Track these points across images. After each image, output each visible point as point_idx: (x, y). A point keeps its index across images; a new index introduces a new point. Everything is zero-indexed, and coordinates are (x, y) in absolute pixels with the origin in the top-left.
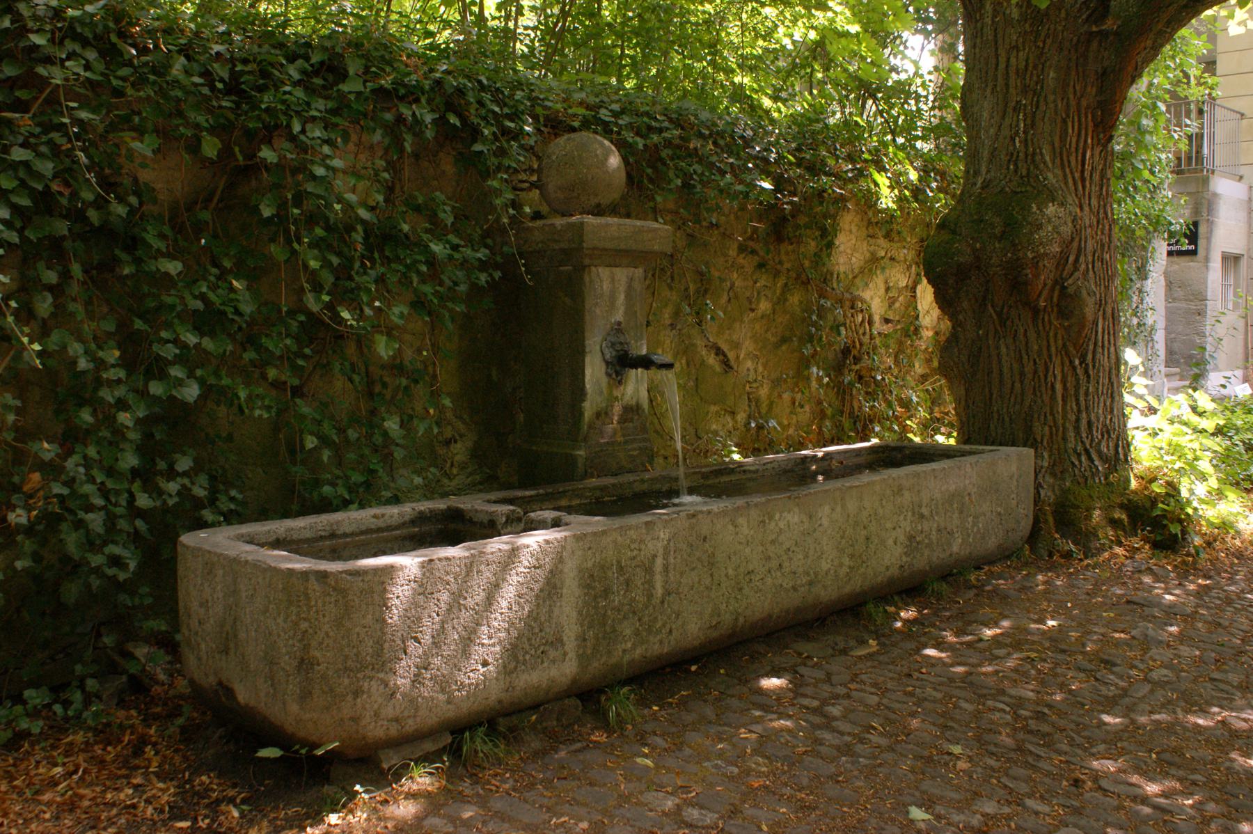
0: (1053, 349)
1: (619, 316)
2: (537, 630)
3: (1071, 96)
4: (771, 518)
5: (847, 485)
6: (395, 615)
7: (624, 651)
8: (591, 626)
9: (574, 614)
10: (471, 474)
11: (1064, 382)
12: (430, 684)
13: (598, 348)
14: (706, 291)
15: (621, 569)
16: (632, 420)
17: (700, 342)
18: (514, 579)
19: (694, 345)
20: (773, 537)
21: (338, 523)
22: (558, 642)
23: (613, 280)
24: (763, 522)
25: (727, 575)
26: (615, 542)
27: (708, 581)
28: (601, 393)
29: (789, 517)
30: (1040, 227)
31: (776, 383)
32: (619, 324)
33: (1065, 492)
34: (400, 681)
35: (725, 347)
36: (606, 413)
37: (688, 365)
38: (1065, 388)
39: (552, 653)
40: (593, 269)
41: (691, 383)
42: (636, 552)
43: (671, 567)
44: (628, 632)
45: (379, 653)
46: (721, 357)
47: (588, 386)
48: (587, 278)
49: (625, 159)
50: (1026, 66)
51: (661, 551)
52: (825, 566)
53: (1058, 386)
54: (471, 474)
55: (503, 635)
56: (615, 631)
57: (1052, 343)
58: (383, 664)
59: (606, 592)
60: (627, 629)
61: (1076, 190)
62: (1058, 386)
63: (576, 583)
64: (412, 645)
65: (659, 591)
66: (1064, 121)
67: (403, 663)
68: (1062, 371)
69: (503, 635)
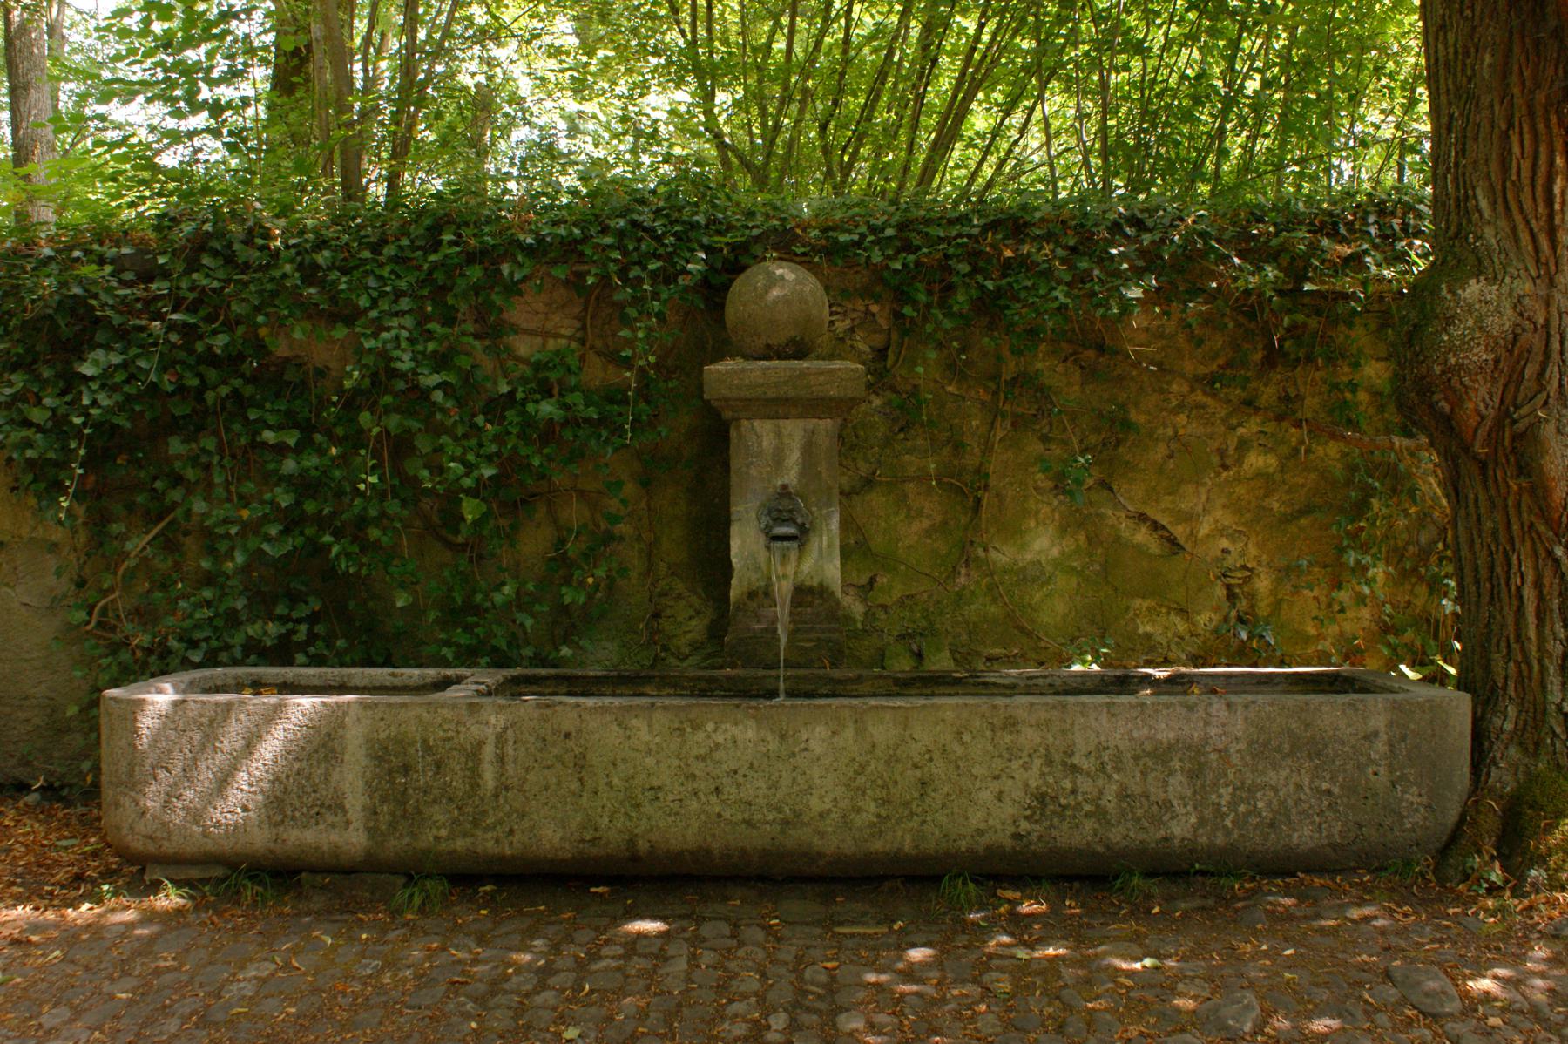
0: (1515, 528)
1: (791, 476)
2: (309, 790)
3: (1516, 91)
6: (144, 742)
7: (437, 838)
8: (384, 800)
9: (360, 784)
10: (709, 656)
11: (1538, 584)
12: (182, 814)
15: (428, 749)
16: (811, 605)
18: (279, 733)
20: (702, 751)
21: (349, 676)
22: (339, 807)
23: (778, 434)
24: (681, 730)
25: (609, 784)
26: (419, 718)
27: (575, 786)
30: (1449, 321)
31: (1286, 572)
32: (784, 487)
33: (1532, 778)
34: (150, 804)
38: (1541, 598)
39: (330, 818)
40: (745, 422)
42: (450, 734)
43: (509, 760)
45: (131, 774)
47: (734, 561)
48: (733, 434)
50: (1456, 53)
51: (491, 739)
52: (816, 804)
53: (1529, 593)
54: (709, 656)
55: (266, 786)
56: (420, 812)
57: (1514, 520)
58: (134, 785)
59: (406, 769)
60: (439, 814)
61: (1537, 250)
62: (1529, 593)
63: (363, 751)
64: (162, 774)
66: (1505, 136)
67: (153, 788)
68: (1536, 568)
69: (266, 786)
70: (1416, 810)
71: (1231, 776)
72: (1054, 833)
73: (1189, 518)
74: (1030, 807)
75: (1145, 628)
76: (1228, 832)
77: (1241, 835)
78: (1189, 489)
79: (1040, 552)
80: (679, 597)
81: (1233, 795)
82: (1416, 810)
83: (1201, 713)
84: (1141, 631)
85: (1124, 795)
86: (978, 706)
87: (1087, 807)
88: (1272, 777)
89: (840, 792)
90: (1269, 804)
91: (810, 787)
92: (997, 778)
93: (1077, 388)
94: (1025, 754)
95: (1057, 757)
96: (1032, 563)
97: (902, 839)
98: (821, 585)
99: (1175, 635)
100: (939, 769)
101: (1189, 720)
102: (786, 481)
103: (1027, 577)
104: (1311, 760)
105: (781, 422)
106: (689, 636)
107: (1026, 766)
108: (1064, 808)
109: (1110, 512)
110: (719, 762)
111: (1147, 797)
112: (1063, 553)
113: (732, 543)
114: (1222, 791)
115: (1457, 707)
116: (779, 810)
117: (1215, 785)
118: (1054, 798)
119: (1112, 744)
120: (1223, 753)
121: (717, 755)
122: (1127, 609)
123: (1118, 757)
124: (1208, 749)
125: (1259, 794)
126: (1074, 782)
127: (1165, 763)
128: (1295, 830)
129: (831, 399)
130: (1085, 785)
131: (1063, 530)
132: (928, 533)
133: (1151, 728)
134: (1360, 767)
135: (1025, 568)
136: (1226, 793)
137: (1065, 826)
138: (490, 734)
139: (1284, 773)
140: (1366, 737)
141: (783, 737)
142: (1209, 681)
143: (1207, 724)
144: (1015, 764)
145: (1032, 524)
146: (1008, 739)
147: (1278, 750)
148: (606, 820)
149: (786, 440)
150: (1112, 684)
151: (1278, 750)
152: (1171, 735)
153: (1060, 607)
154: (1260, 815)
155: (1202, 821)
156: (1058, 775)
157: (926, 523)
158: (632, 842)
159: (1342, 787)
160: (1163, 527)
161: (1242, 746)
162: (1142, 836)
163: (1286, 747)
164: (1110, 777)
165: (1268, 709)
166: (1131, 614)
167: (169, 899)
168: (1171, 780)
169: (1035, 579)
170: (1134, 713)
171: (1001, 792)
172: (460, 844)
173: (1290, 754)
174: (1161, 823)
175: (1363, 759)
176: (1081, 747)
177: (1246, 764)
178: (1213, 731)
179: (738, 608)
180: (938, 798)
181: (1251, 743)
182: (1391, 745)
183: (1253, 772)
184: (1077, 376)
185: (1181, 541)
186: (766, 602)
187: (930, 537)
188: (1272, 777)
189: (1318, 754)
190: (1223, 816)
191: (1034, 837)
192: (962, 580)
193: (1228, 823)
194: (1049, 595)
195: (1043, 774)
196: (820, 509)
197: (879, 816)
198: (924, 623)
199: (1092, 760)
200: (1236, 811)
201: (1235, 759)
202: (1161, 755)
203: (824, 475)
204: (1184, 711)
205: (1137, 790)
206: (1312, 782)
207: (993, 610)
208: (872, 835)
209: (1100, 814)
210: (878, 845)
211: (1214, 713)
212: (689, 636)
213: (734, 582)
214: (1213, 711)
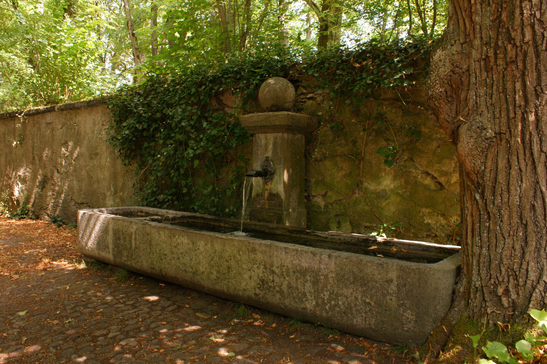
1: (269, 154)
4: (174, 236)
5: (217, 235)
16: (274, 200)
20: (175, 245)
22: (108, 247)
23: (266, 139)
28: (260, 186)
29: (183, 239)
32: (266, 157)
36: (262, 195)
40: (257, 135)
44: (125, 254)
65: (134, 246)
70: (410, 322)
71: (329, 288)
72: (267, 296)
73: (445, 174)
74: (259, 284)
75: (427, 221)
76: (327, 312)
77: (333, 314)
78: (447, 161)
81: (329, 296)
82: (410, 322)
83: (318, 257)
84: (425, 222)
85: (290, 287)
86: (244, 241)
87: (277, 289)
88: (345, 291)
89: (207, 266)
90: (344, 303)
91: (200, 263)
92: (250, 270)
93: (400, 118)
94: (258, 263)
95: (268, 266)
96: (383, 190)
97: (222, 287)
98: (277, 193)
99: (441, 225)
100: (233, 263)
101: (313, 260)
102: (268, 155)
103: (382, 195)
104: (362, 287)
105: (267, 134)
107: (258, 268)
108: (270, 287)
109: (414, 171)
110: (179, 249)
111: (298, 289)
112: (395, 187)
114: (325, 293)
115: (433, 274)
116: (192, 268)
117: (322, 290)
118: (267, 283)
119: (286, 264)
120: (326, 277)
121: (179, 247)
122: (420, 212)
123: (288, 270)
124: (320, 274)
125: (340, 298)
126: (273, 277)
127: (304, 276)
128: (355, 318)
130: (277, 280)
131: (395, 178)
132: (345, 176)
133: (300, 260)
134: (384, 295)
135: (379, 192)
136: (327, 294)
137: (270, 294)
138: (133, 230)
139: (351, 291)
140: (387, 281)
141: (193, 243)
142: (401, 246)
143: (320, 263)
144: (255, 266)
145: (383, 174)
146: (253, 256)
147: (348, 279)
148: (155, 263)
150: (362, 242)
151: (348, 279)
152: (307, 265)
153: (393, 209)
154: (340, 307)
155: (317, 304)
156: (268, 273)
157: (344, 173)
158: (161, 270)
159: (375, 302)
160: (436, 178)
161: (333, 275)
162: (296, 305)
163: (352, 279)
164: (285, 278)
165: (345, 260)
166: (421, 214)
167: (83, 266)
168: (306, 284)
169: (383, 197)
170: (294, 253)
171: (251, 276)
172: (129, 263)
173: (353, 283)
174: (302, 301)
175: (385, 292)
176: (276, 264)
177: (335, 284)
178: (322, 266)
180: (233, 273)
181: (337, 274)
182: (398, 286)
183: (337, 287)
184: (401, 114)
185: (444, 184)
186: (262, 198)
187: (345, 178)
188: (345, 291)
189: (365, 285)
190: (326, 304)
191: (261, 296)
192: (357, 195)
193: (327, 307)
194: (388, 204)
195: (263, 272)
197: (217, 277)
198: (344, 211)
199: (279, 270)
200: (330, 303)
201: (331, 280)
202: (303, 272)
203: (279, 154)
204: (312, 255)
205: (294, 285)
206: (362, 297)
207: (366, 208)
208: (215, 283)
209: (281, 292)
210: (217, 287)
211: (323, 258)
214: (323, 257)
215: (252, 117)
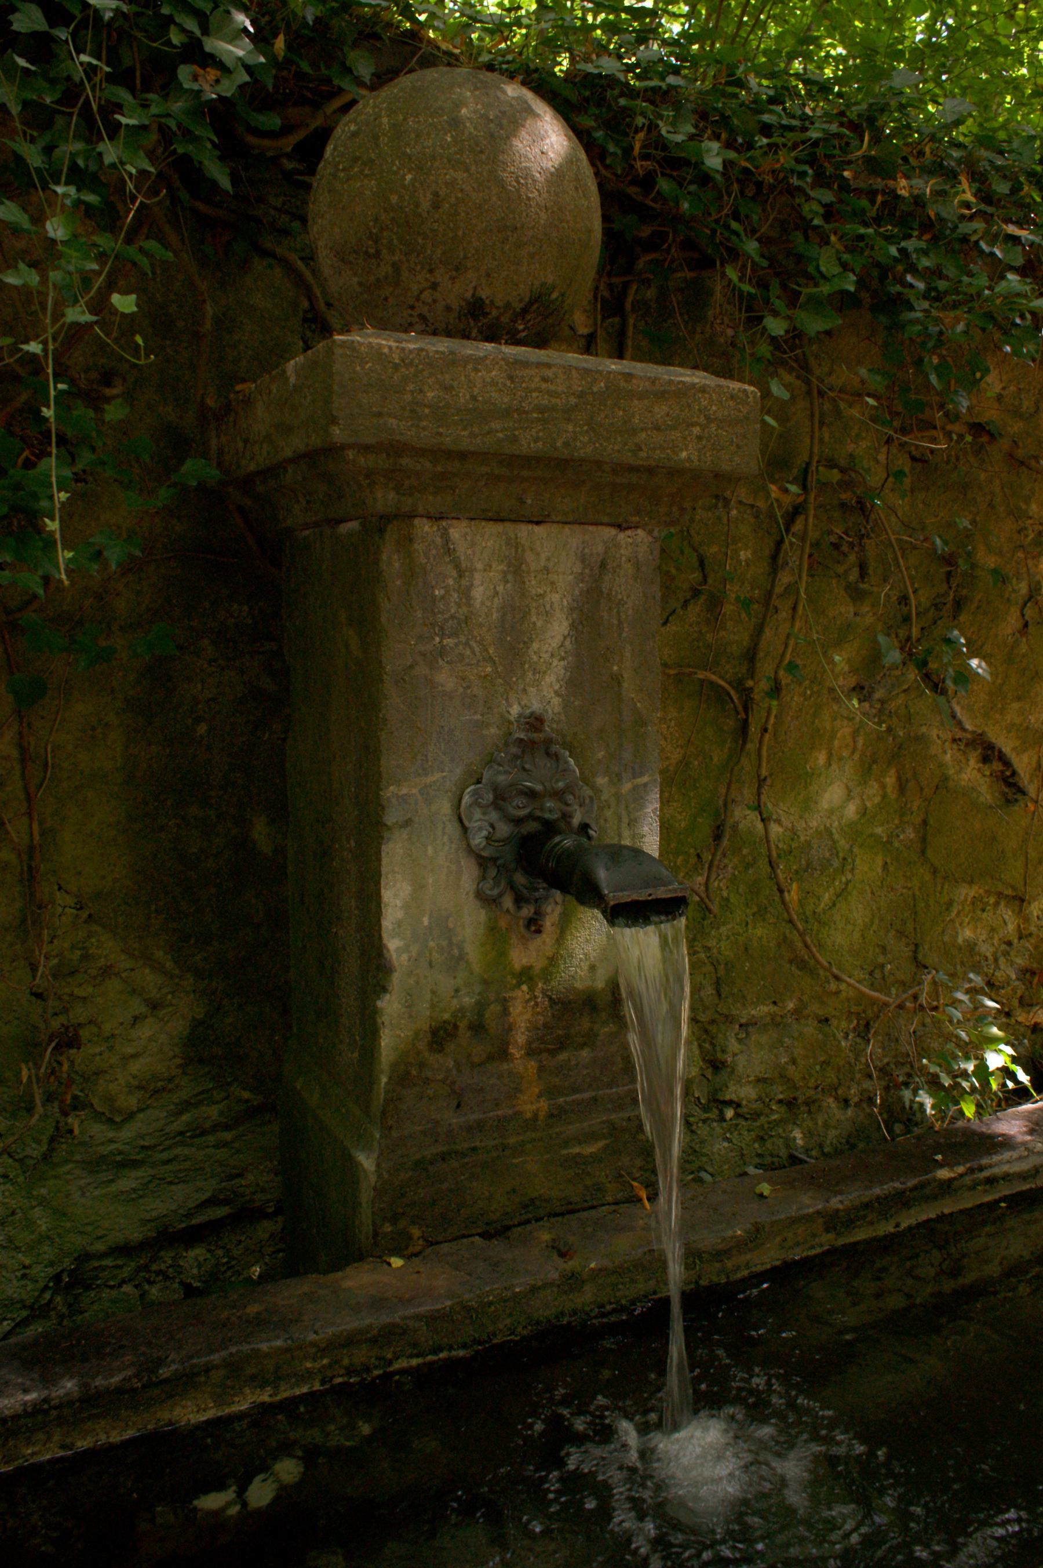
10: (186, 1106)
13: (445, 807)
14: (959, 605)
17: (936, 732)
19: (921, 740)
28: (456, 960)
32: (535, 722)
35: (1006, 744)
37: (902, 787)
40: (424, 527)
41: (910, 834)
46: (997, 766)
47: (393, 944)
48: (391, 562)
49: (579, 133)
54: (186, 1106)
79: (831, 812)
80: (107, 972)
105: (524, 531)
106: (135, 1067)
113: (387, 895)
122: (950, 904)
129: (675, 472)
149: (534, 587)
179: (402, 1078)
196: (617, 779)
212: (135, 1067)
213: (390, 1005)
215: (453, 361)
